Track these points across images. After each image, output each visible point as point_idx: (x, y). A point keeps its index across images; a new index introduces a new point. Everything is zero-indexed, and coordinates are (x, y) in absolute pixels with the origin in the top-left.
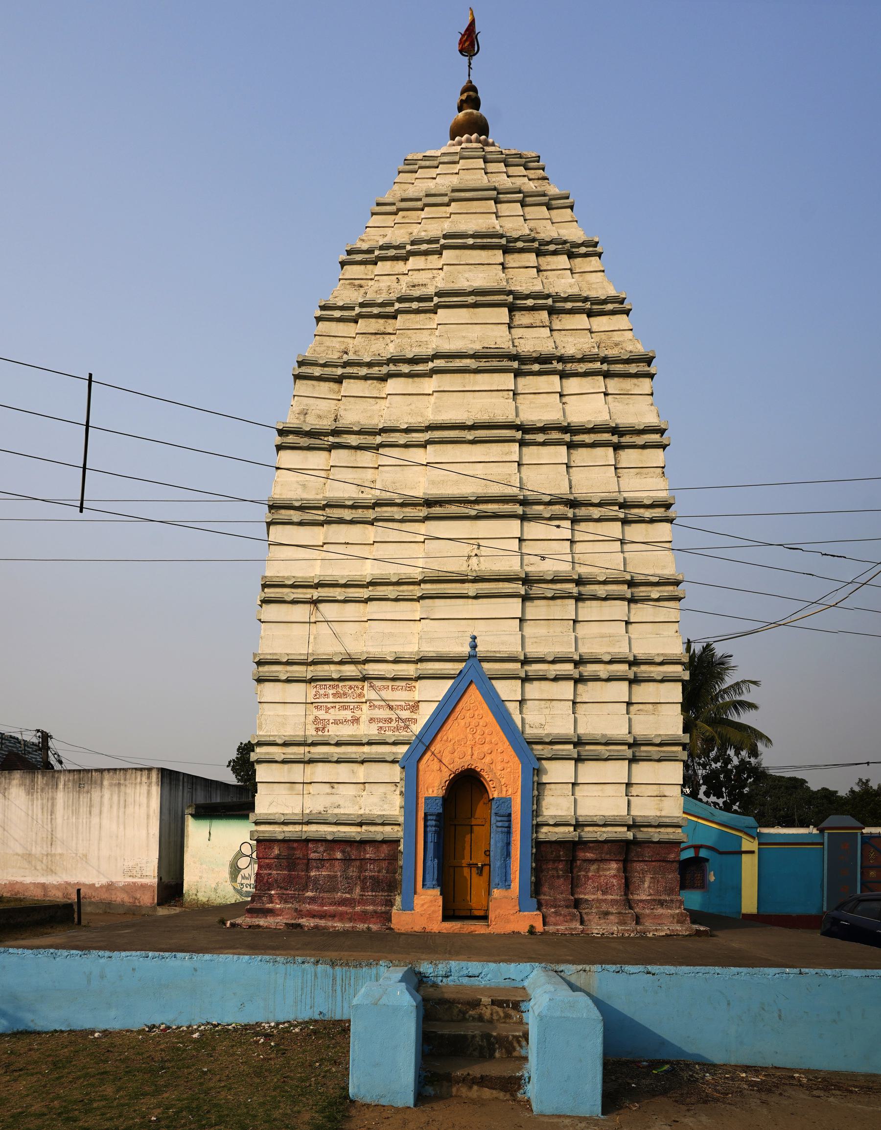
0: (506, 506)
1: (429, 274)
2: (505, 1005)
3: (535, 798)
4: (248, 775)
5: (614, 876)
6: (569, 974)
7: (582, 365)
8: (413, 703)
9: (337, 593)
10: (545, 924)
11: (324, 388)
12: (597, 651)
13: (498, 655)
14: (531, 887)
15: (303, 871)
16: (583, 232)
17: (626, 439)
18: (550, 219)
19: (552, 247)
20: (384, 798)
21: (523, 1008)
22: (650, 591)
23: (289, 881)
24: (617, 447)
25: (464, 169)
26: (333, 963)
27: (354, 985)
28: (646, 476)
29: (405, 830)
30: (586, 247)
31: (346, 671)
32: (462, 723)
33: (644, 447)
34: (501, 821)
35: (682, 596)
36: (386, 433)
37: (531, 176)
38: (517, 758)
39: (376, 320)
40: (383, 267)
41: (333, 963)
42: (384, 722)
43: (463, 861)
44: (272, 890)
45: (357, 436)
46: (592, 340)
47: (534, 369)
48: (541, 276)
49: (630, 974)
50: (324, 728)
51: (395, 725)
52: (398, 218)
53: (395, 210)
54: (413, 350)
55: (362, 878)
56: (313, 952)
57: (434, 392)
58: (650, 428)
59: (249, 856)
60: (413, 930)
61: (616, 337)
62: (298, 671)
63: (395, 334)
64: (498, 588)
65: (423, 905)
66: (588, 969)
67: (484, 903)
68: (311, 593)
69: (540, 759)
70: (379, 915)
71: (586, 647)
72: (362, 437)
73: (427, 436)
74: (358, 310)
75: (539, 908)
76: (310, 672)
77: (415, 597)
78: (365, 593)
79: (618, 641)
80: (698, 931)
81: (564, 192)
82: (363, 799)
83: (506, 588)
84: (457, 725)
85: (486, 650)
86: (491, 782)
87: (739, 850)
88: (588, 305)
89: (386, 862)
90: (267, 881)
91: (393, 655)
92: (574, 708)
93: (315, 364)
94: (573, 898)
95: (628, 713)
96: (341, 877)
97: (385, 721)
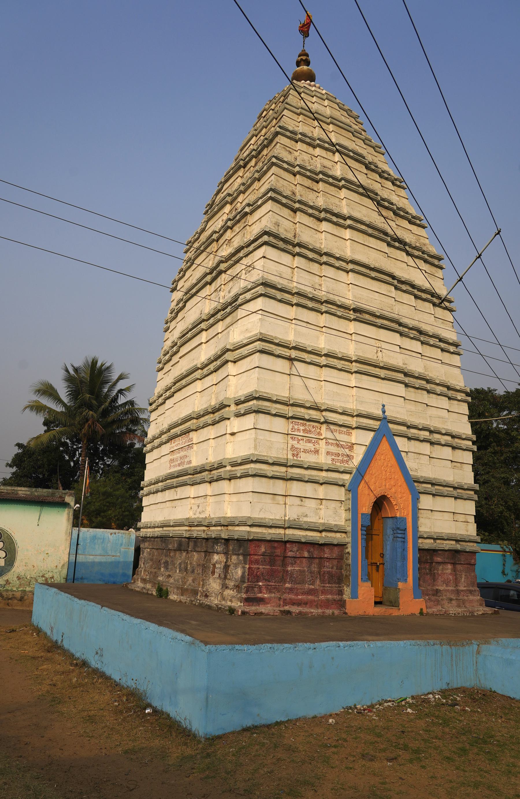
0: (392, 324)
8: (350, 444)
15: (280, 566)
23: (272, 574)
50: (297, 455)
52: (301, 118)
53: (299, 112)
65: (363, 594)
76: (290, 411)
89: (336, 560)
90: (256, 574)
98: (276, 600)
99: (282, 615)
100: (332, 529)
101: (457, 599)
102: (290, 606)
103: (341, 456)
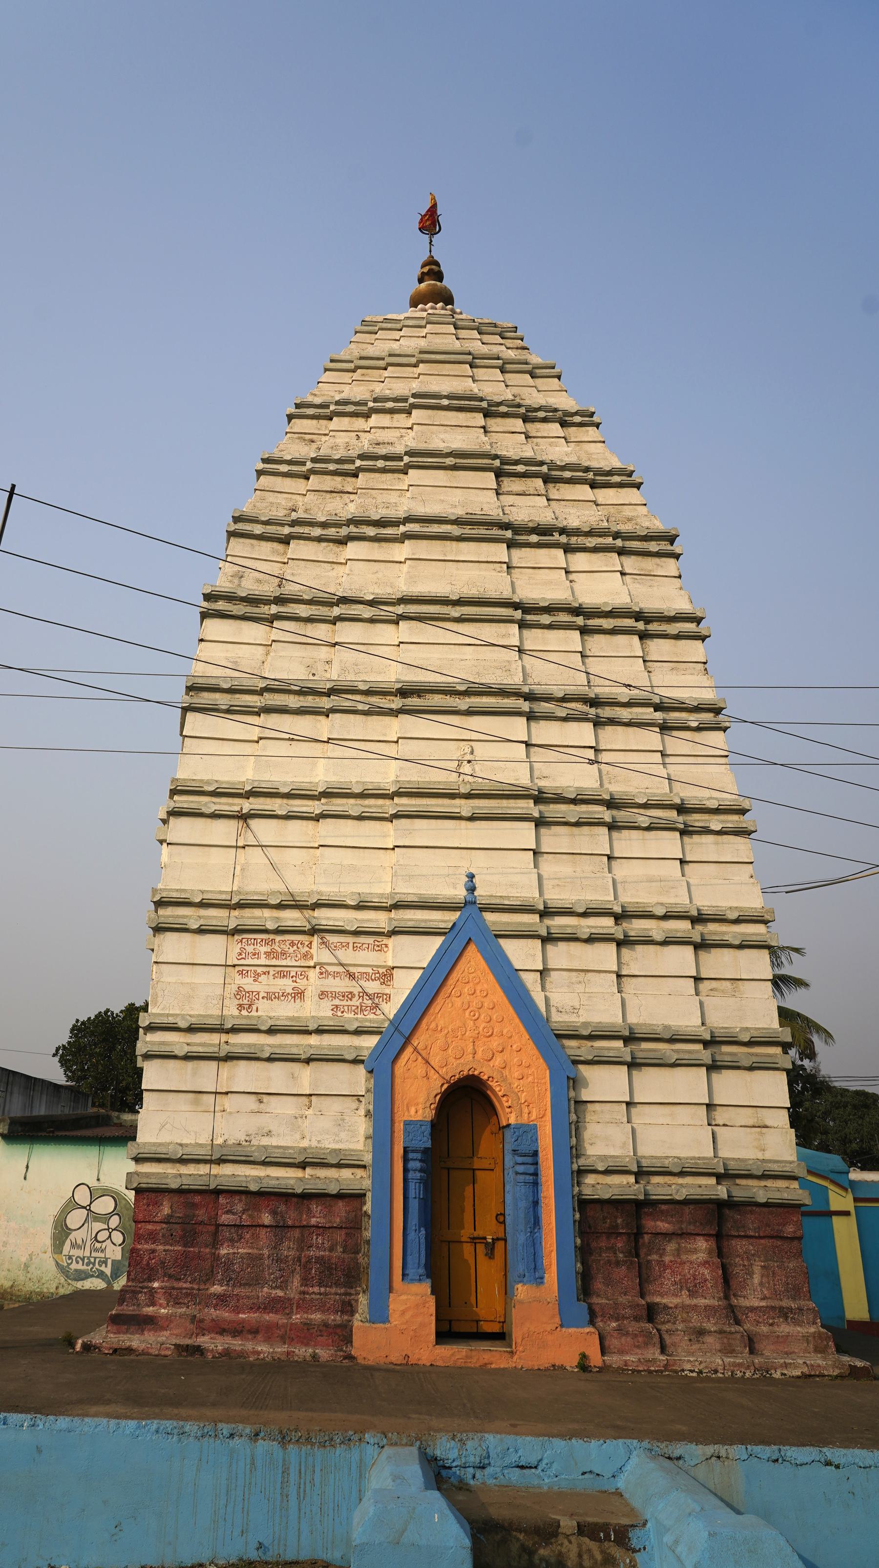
0: (506, 701)
1: (397, 433)
2: (602, 1535)
3: (573, 1127)
4: (83, 1070)
5: (705, 1263)
6: (692, 1463)
7: (590, 539)
8: (384, 970)
9: (277, 805)
12: (645, 901)
13: (506, 902)
14: (577, 1281)
15: (206, 1246)
17: (654, 627)
18: (535, 387)
19: (541, 414)
20: (340, 1122)
21: (635, 1543)
22: (709, 821)
24: (644, 636)
26: (284, 1438)
27: (321, 1483)
28: (684, 672)
31: (286, 919)
32: (458, 1002)
33: (678, 637)
34: (523, 1164)
35: (753, 829)
36: (346, 604)
37: (508, 346)
38: (542, 1061)
39: (332, 477)
40: (337, 423)
41: (284, 1438)
42: (341, 998)
43: (462, 1232)
44: (154, 1280)
48: (530, 442)
49: (797, 1465)
50: (250, 1005)
51: (358, 1004)
52: (357, 375)
53: (353, 367)
54: (380, 511)
55: (303, 1260)
56: (244, 1412)
57: (406, 559)
59: (85, 1208)
60: (388, 1360)
61: (628, 512)
63: (356, 493)
64: (502, 808)
65: (403, 1313)
66: (723, 1453)
67: (500, 1309)
68: (238, 805)
69: (575, 1062)
70: (331, 1330)
71: (629, 894)
72: (314, 607)
73: (400, 609)
74: (309, 465)
75: (592, 1322)
76: (234, 918)
77: (387, 815)
78: (316, 807)
79: (673, 888)
81: (549, 362)
82: (307, 1123)
84: (450, 1005)
85: (488, 894)
86: (505, 1099)
87: (823, 1209)
88: (590, 475)
89: (343, 1232)
91: (356, 897)
92: (619, 984)
94: (643, 1302)
95: (697, 994)
96: (269, 1257)
97: (343, 996)
98: (183, 1320)
99: (181, 1355)
100: (326, 1161)
101: (721, 1332)
102: (213, 1335)
103: (357, 997)
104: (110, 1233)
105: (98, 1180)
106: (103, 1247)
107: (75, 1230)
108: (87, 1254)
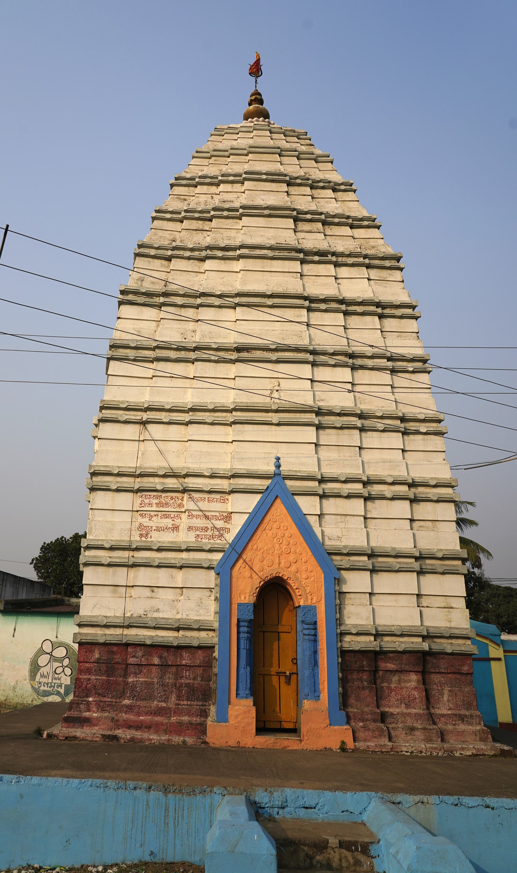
0: (299, 355)
1: (235, 195)
2: (353, 848)
3: (338, 607)
5: (416, 688)
6: (407, 806)
8: (226, 514)
9: (163, 416)
10: (355, 741)
11: (157, 264)
12: (381, 474)
14: (339, 698)
15: (121, 677)
16: (341, 177)
17: (387, 311)
18: (318, 168)
19: (321, 184)
20: (200, 603)
21: (373, 853)
22: (419, 426)
25: (256, 136)
26: (166, 790)
27: (188, 817)
28: (405, 338)
29: (220, 636)
30: (345, 185)
31: (169, 483)
32: (270, 533)
33: (401, 317)
35: (445, 431)
37: (302, 143)
38: (319, 568)
39: (197, 221)
40: (200, 189)
41: (166, 790)
42: (201, 530)
43: (272, 669)
44: (89, 697)
45: (182, 298)
46: (356, 243)
47: (315, 259)
50: (147, 534)
51: (211, 534)
52: (212, 161)
53: (210, 156)
55: (178, 685)
57: (240, 270)
58: (405, 304)
60: (227, 745)
61: (372, 243)
62: (126, 481)
63: (211, 231)
64: (296, 418)
65: (237, 717)
66: (425, 800)
67: (294, 714)
68: (141, 415)
69: (339, 569)
72: (185, 299)
73: (237, 300)
74: (183, 214)
75: (348, 723)
76: (137, 483)
77: (228, 422)
78: (186, 417)
79: (397, 466)
80: (502, 751)
81: (326, 153)
82: (180, 604)
83: (303, 418)
84: (265, 535)
86: (297, 590)
87: (485, 656)
88: (350, 221)
89: (202, 668)
91: (210, 470)
92: (365, 523)
93: (151, 247)
94: (379, 711)
95: (412, 529)
96: (157, 683)
100: (191, 627)
101: (424, 729)
102: (124, 729)
103: (210, 530)
104: (64, 669)
105: (57, 637)
106: (60, 677)
107: (43, 667)
108: (50, 681)
